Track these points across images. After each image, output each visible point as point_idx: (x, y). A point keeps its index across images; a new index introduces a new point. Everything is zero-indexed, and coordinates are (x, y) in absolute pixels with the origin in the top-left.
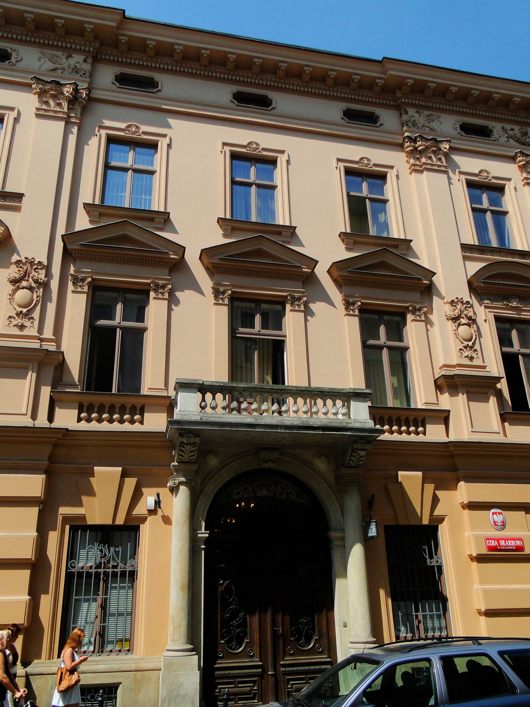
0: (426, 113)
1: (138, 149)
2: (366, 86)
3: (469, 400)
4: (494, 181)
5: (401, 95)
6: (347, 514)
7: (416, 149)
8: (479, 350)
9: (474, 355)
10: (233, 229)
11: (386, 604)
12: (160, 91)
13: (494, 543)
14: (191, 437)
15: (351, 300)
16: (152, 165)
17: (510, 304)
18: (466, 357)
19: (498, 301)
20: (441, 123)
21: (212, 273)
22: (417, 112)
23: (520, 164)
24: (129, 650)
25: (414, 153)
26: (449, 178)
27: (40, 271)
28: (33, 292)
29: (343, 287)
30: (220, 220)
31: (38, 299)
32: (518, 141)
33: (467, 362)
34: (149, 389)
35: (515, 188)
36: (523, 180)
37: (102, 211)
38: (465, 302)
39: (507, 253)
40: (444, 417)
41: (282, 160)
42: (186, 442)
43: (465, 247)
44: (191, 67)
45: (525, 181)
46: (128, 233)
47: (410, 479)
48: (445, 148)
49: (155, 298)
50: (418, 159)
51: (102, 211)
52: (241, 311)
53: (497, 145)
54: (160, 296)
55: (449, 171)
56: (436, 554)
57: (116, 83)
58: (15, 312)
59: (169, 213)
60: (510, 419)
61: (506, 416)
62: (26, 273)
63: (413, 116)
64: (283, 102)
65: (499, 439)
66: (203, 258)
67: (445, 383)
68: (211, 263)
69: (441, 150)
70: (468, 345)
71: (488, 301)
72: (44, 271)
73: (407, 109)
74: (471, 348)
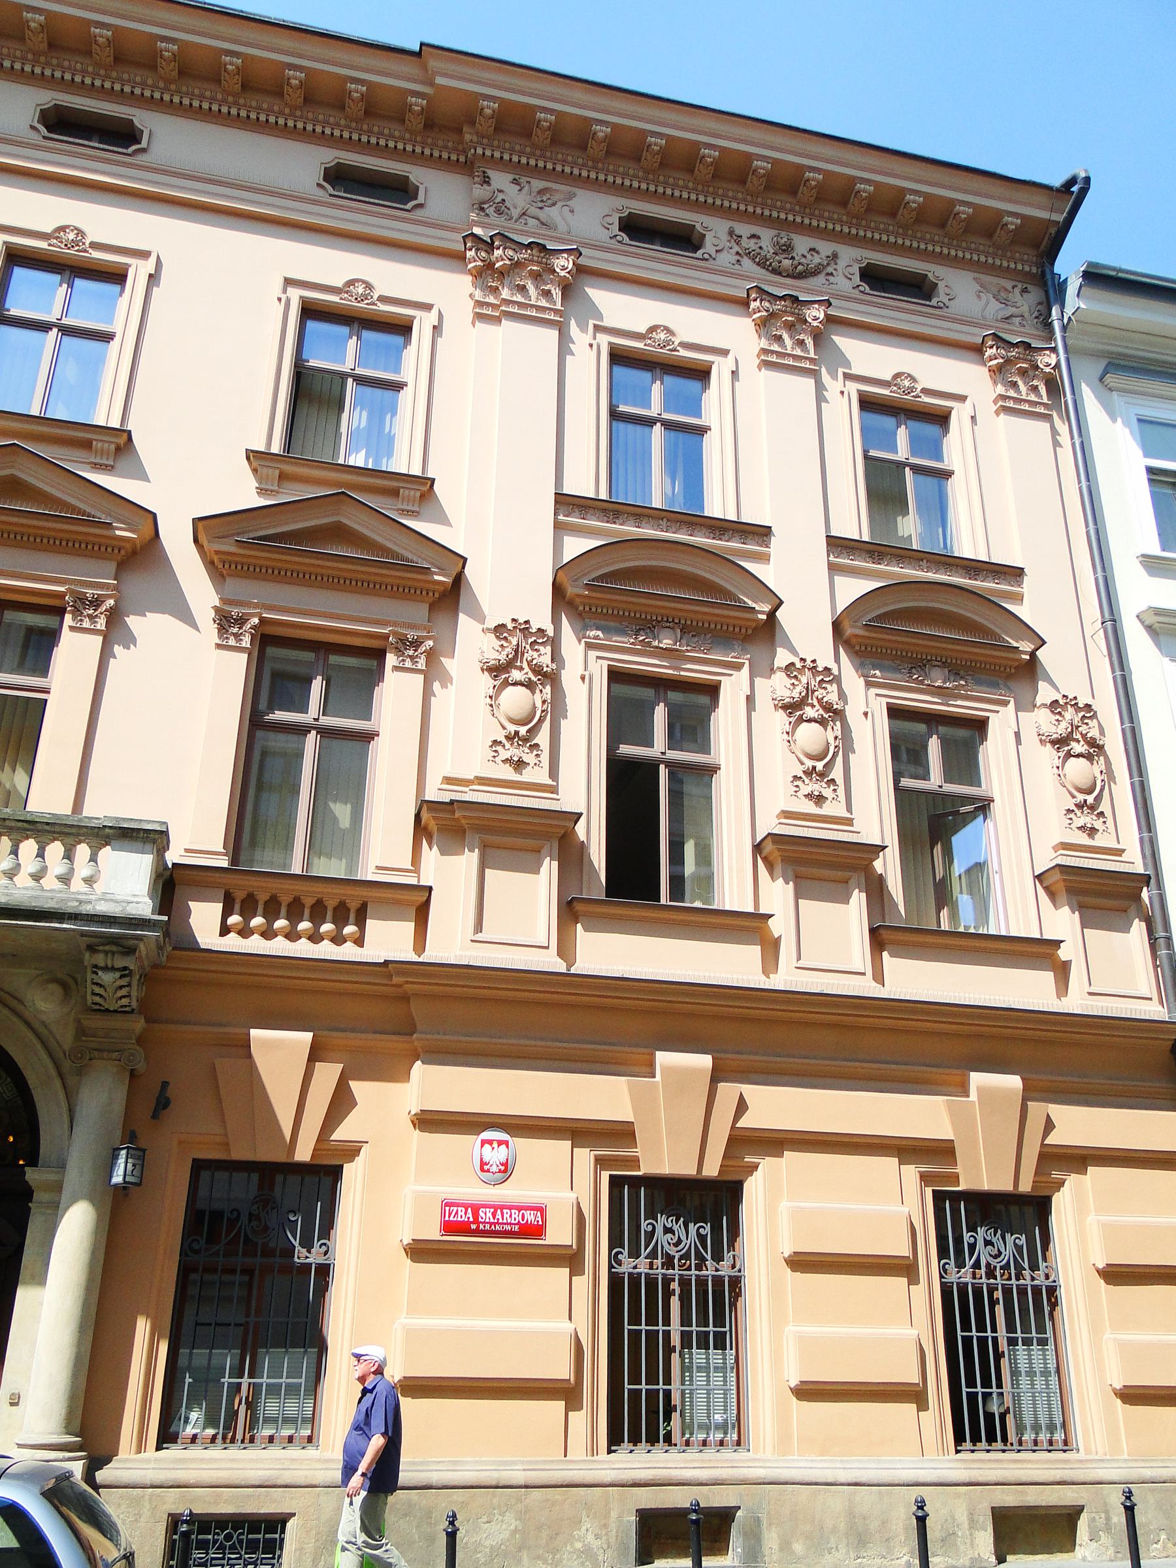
0: (538, 184)
1: (367, 335)
2: (378, 109)
3: (1084, 925)
4: (926, 399)
5: (475, 139)
6: (82, 1129)
7: (490, 266)
8: (840, 781)
9: (1098, 824)
10: (283, 477)
11: (146, 1352)
12: (144, 150)
13: (462, 1215)
14: (113, 953)
15: (235, 611)
16: (397, 370)
17: (656, 643)
18: (505, 761)
19: (623, 632)
20: (572, 211)
21: (222, 576)
22: (515, 182)
23: (992, 363)
24: (310, 1439)
25: (486, 274)
26: (820, 388)
27: (541, 648)
28: (533, 693)
29: (228, 580)
30: (252, 456)
31: (545, 707)
32: (763, 264)
33: (1083, 839)
34: (378, 868)
35: (973, 418)
36: (995, 402)
37: (289, 468)
38: (820, 669)
39: (846, 547)
40: (417, 905)
41: (423, 325)
42: (102, 964)
43: (836, 544)
44: (60, 66)
45: (1000, 403)
46: (345, 521)
47: (279, 1051)
48: (816, 319)
49: (396, 668)
50: (495, 291)
51: (289, 468)
52: (281, 667)
53: (939, 318)
54: (408, 664)
55: (1055, 415)
56: (1045, 1259)
57: (325, 184)
58: (504, 733)
59: (433, 481)
60: (892, 943)
61: (579, 907)
62: (516, 651)
63: (501, 191)
64: (170, 138)
65: (865, 987)
66: (203, 539)
67: (777, 853)
68: (217, 552)
69: (1037, 367)
70: (1085, 801)
71: (599, 633)
72: (548, 649)
73: (490, 173)
74: (1092, 808)
